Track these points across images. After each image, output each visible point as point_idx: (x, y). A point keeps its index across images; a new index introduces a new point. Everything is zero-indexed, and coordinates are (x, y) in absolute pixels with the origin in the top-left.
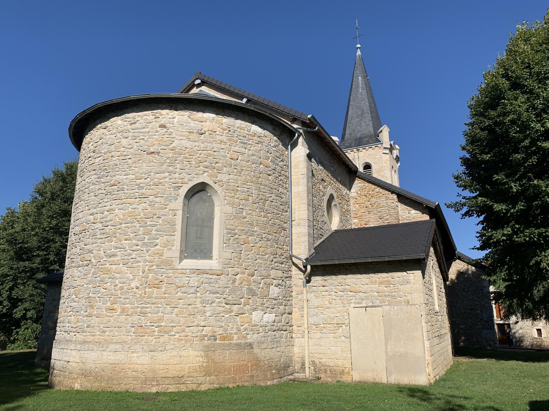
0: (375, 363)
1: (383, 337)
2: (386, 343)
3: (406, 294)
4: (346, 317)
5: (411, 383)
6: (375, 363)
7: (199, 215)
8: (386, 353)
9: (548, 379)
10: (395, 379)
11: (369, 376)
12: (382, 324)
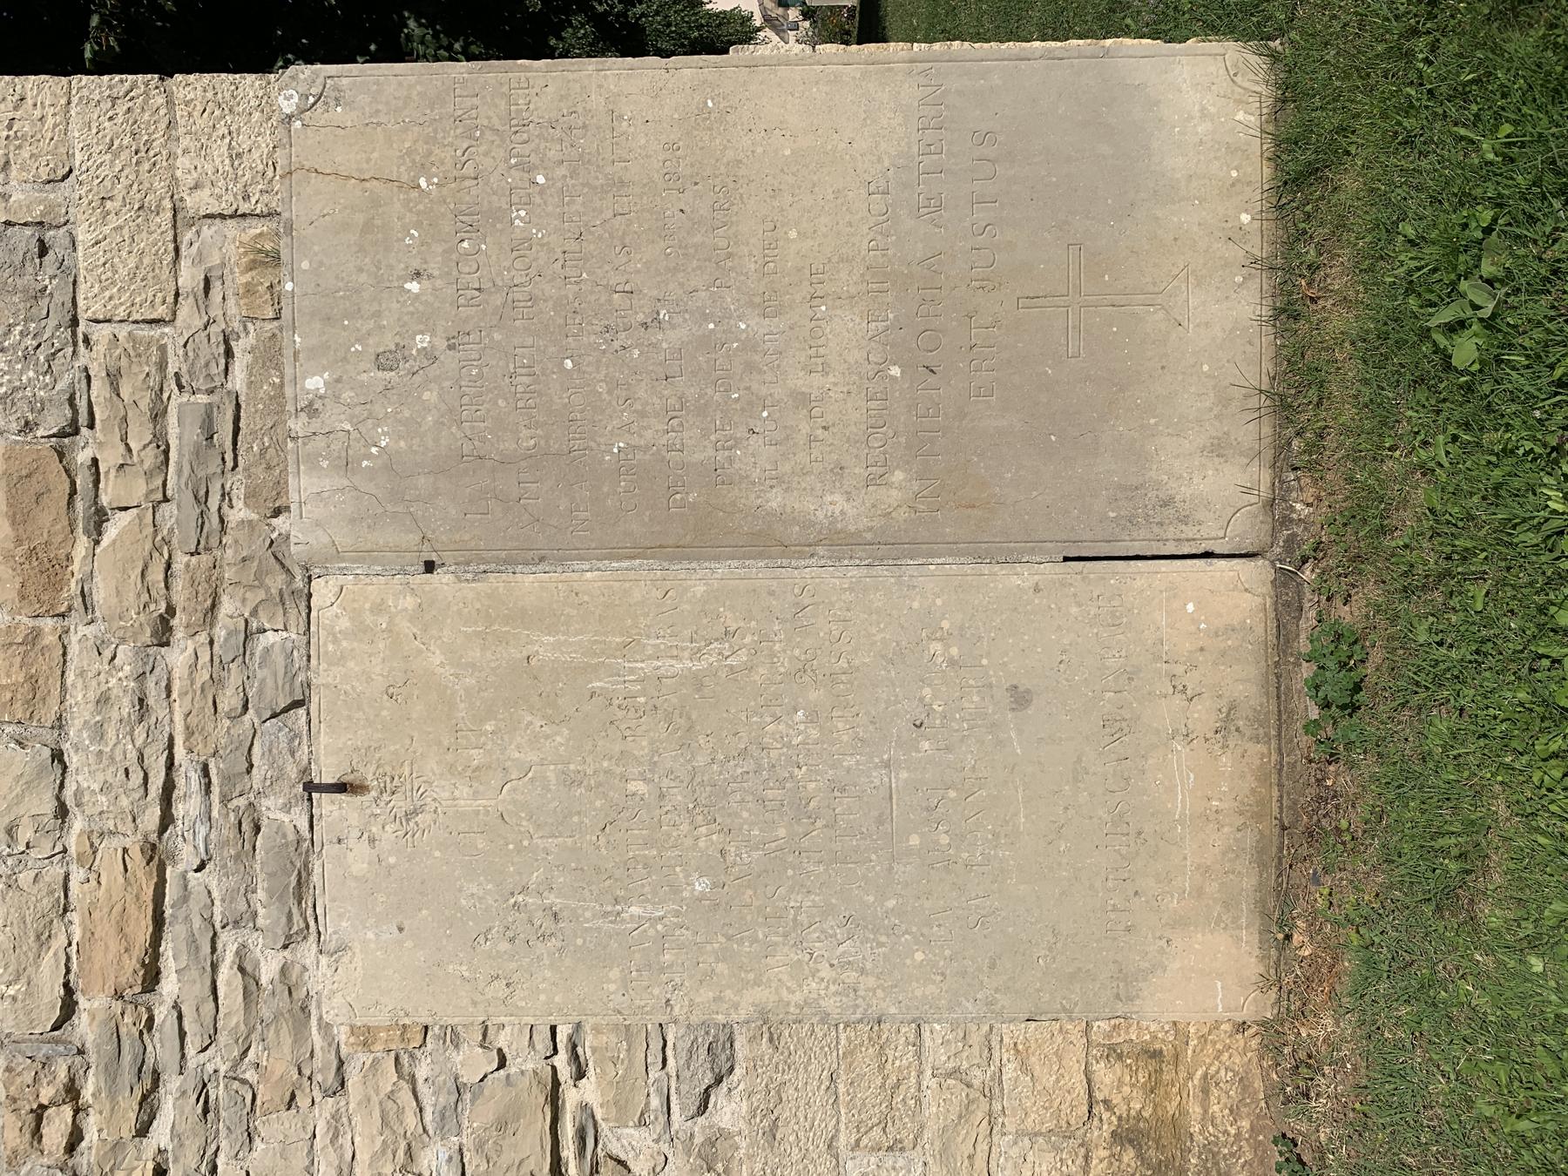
0: (1020, 699)
2: (771, 542)
3: (189, 277)
5: (1258, 247)
6: (1020, 699)
8: (886, 546)
9: (1045, 1175)
10: (1218, 449)
11: (1204, 788)
12: (528, 583)
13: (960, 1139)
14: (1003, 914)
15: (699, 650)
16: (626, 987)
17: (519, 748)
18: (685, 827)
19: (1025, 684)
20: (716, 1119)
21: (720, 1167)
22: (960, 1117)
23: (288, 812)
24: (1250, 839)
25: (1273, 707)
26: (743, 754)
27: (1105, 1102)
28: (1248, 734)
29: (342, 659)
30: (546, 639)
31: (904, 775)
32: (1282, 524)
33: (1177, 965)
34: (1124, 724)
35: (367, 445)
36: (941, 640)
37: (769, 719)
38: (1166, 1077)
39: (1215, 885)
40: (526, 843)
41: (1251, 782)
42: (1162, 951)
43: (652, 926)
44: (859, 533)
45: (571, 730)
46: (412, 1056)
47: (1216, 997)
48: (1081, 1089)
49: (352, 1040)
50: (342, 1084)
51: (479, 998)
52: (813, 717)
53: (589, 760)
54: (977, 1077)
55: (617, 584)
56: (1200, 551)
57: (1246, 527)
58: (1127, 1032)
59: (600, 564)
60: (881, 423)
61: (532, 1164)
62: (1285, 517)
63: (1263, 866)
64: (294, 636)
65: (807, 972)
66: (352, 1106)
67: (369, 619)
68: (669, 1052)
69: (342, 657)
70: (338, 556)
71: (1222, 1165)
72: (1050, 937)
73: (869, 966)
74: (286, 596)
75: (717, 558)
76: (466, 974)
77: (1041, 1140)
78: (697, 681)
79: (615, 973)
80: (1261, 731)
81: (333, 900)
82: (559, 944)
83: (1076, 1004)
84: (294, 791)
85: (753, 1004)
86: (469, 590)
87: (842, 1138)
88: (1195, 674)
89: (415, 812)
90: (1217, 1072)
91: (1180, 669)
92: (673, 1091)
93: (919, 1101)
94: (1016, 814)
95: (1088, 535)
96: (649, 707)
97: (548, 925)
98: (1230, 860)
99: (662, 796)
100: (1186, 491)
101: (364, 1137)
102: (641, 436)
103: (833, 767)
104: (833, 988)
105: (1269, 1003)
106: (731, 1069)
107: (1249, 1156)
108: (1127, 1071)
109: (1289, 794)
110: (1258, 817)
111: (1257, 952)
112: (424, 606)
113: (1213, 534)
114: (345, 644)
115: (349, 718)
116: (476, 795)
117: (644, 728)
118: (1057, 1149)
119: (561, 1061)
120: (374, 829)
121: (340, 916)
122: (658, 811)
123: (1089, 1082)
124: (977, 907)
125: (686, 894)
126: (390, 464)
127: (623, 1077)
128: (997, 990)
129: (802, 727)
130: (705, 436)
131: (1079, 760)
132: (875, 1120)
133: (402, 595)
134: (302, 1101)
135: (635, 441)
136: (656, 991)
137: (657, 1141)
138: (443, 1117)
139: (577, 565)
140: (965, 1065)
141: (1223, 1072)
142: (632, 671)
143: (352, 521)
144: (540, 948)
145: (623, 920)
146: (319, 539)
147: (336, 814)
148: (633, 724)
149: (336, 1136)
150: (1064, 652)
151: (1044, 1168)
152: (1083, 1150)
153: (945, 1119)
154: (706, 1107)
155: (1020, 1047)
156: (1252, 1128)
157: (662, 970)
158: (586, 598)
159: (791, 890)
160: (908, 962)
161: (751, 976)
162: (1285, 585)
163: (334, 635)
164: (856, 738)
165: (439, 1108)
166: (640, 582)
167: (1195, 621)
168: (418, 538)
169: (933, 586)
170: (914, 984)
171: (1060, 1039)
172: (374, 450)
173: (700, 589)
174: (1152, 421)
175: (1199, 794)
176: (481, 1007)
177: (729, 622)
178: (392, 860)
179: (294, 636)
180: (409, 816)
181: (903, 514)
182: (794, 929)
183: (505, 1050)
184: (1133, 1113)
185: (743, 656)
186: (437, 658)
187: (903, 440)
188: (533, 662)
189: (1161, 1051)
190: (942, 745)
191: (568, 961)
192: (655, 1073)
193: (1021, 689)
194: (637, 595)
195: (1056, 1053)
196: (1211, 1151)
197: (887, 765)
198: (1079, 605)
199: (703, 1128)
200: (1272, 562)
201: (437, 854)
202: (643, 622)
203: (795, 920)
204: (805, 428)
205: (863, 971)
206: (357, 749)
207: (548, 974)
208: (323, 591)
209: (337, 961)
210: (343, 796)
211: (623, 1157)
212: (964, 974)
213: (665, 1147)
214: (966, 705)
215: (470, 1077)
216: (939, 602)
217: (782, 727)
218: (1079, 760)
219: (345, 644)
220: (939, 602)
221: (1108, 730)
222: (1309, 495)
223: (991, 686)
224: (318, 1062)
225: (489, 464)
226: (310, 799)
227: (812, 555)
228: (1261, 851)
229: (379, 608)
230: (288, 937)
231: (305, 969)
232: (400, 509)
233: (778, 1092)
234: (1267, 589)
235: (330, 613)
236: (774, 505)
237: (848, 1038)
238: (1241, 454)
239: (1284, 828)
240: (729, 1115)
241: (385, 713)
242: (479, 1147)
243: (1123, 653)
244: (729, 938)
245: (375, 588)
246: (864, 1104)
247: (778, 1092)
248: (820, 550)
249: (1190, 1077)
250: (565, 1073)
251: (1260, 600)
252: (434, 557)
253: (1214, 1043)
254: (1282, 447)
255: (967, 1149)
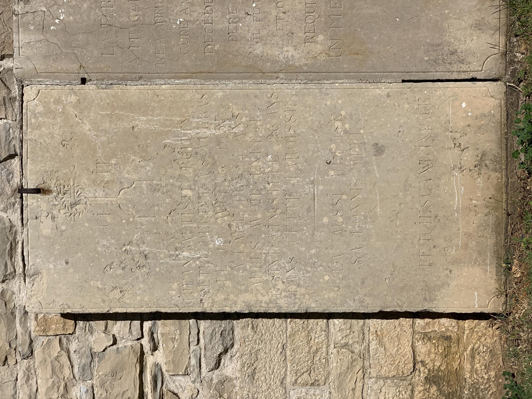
0: (379, 150)
1: (219, 91)
2: (257, 71)
4: (97, 336)
6: (379, 150)
7: (229, 371)
8: (314, 74)
10: (479, 26)
12: (133, 90)
13: (348, 380)
14: (368, 256)
15: (219, 125)
16: (180, 293)
17: (128, 172)
18: (211, 213)
19: (381, 142)
20: (224, 371)
21: (226, 396)
22: (348, 368)
23: (6, 212)
24: (491, 220)
25: (504, 154)
26: (241, 176)
27: (422, 362)
28: (491, 168)
29: (39, 127)
30: (142, 118)
31: (321, 187)
32: (510, 64)
33: (455, 283)
34: (430, 162)
35: (54, 18)
36: (341, 120)
37: (254, 159)
38: (453, 350)
39: (474, 243)
40: (131, 220)
41: (492, 192)
42: (447, 276)
43: (193, 262)
44: (301, 67)
45: (154, 164)
46: (68, 339)
47: (474, 300)
48: (410, 355)
49: (37, 329)
50: (32, 354)
51: (106, 298)
52: (275, 159)
53: (163, 179)
54: (357, 348)
55: (178, 91)
56: (470, 77)
57: (492, 66)
58: (433, 327)
59: (169, 81)
60: (312, 10)
61: (129, 394)
62: (511, 60)
63: (498, 233)
64: (10, 122)
65: (271, 286)
66: (36, 364)
67: (53, 107)
68: (201, 336)
69: (39, 125)
70: (38, 75)
71: (481, 394)
72: (391, 268)
73: (302, 283)
74: (7, 101)
75: (229, 79)
76: (100, 286)
77: (389, 381)
78: (218, 140)
79: (175, 286)
80: (498, 166)
81: (32, 248)
82: (147, 271)
83: (404, 303)
84: (10, 201)
85: (244, 302)
86: (103, 93)
87: (288, 379)
88: (466, 138)
89: (75, 204)
90: (479, 347)
91: (458, 135)
92: (202, 356)
93: (327, 360)
94: (376, 207)
95: (414, 69)
96: (193, 153)
97: (142, 261)
98: (481, 231)
99: (199, 197)
100: (463, 47)
101: (43, 380)
102: (191, 15)
103: (286, 183)
104: (284, 294)
105: (501, 303)
106: (232, 345)
107: (494, 390)
108: (433, 346)
109: (511, 198)
110: (496, 209)
111: (495, 277)
112: (81, 101)
113: (476, 69)
114: (40, 119)
115: (43, 156)
116: (106, 195)
117: (190, 163)
118: (398, 386)
119: (146, 342)
120: (54, 212)
121: (36, 256)
122: (197, 205)
123: (414, 352)
124: (356, 253)
125: (211, 246)
126: (65, 29)
127: (177, 348)
128: (365, 295)
129: (270, 163)
130: (224, 16)
131: (407, 180)
132: (305, 369)
133: (69, 96)
134: (11, 361)
135: (188, 18)
136: (196, 295)
137: (194, 382)
138: (84, 370)
139: (158, 81)
140: (351, 342)
141: (481, 347)
142: (185, 135)
143: (45, 57)
144: (138, 272)
145: (179, 259)
146: (29, 66)
147: (35, 204)
148: (185, 161)
149: (28, 380)
150: (401, 126)
151: (390, 395)
152: (410, 387)
153: (341, 369)
154: (219, 365)
155: (379, 333)
156: (496, 376)
157: (199, 284)
158: (162, 98)
159: (264, 244)
160: (321, 280)
161: (243, 288)
162: (511, 94)
163: (35, 115)
164: (297, 169)
165: (82, 365)
166: (190, 91)
167: (466, 112)
168: (78, 66)
169: (337, 94)
170: (324, 292)
171: (399, 330)
172: (57, 21)
173: (220, 94)
174: (446, 12)
175: (466, 197)
176: (107, 303)
177: (234, 111)
178: (63, 228)
179: (10, 122)
180: (73, 205)
181: (323, 57)
182: (265, 264)
183: (117, 335)
184: (436, 367)
185: (241, 128)
186: (87, 127)
187: (323, 19)
188: (135, 130)
189: (450, 337)
190: (340, 172)
191: (152, 280)
192: (193, 348)
193: (380, 145)
194: (188, 97)
195: (397, 336)
196: (475, 387)
197: (313, 182)
198: (409, 103)
199: (218, 375)
200: (505, 83)
201: (86, 225)
202: (191, 110)
203: (265, 259)
204: (274, 12)
205: (299, 285)
206: (46, 171)
207: (141, 286)
208: (29, 92)
209: (33, 280)
210: (38, 195)
211: (176, 392)
212: (349, 287)
213: (198, 385)
214: (352, 153)
215: (97, 349)
216: (340, 102)
217: (260, 163)
218: (407, 180)
219: (40, 119)
220: (340, 102)
221: (421, 165)
222: (522, 49)
223: (365, 143)
224: (20, 341)
225: (114, 29)
226: (22, 198)
227: (277, 78)
228: (497, 225)
229: (58, 101)
230: (5, 276)
231: (13, 293)
232: (69, 51)
233: (256, 355)
234: (502, 96)
235: (33, 103)
236: (258, 52)
237: (292, 327)
238: (490, 29)
239: (509, 215)
240: (231, 369)
241: (60, 154)
242: (102, 385)
243: (430, 128)
244: (232, 268)
245: (56, 92)
246: (299, 361)
247: (256, 355)
248: (281, 75)
249: (465, 350)
250: (147, 347)
251: (498, 101)
252: (86, 76)
253: (477, 332)
254: (510, 26)
255: (352, 385)
